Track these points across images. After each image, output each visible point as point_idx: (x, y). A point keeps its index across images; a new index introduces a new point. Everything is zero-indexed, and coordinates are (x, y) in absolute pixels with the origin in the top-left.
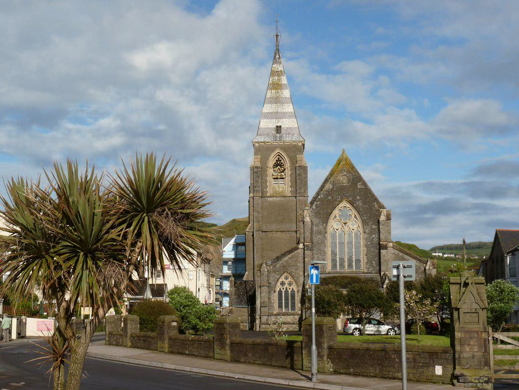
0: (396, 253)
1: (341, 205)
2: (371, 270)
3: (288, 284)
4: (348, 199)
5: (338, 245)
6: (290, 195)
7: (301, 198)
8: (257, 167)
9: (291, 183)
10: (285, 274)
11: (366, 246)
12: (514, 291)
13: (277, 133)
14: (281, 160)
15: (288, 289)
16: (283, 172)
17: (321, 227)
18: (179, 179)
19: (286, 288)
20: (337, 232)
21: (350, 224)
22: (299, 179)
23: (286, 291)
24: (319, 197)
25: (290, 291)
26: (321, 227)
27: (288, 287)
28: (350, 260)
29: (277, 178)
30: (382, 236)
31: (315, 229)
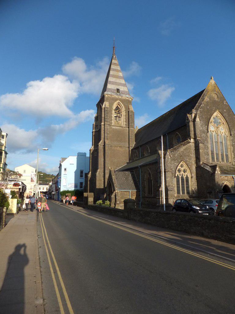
1: (215, 114)
3: (183, 171)
7: (132, 128)
9: (126, 120)
13: (117, 92)
15: (184, 176)
18: (104, 64)
19: (182, 174)
23: (182, 177)
24: (201, 106)
25: (185, 177)
27: (184, 174)
28: (222, 155)
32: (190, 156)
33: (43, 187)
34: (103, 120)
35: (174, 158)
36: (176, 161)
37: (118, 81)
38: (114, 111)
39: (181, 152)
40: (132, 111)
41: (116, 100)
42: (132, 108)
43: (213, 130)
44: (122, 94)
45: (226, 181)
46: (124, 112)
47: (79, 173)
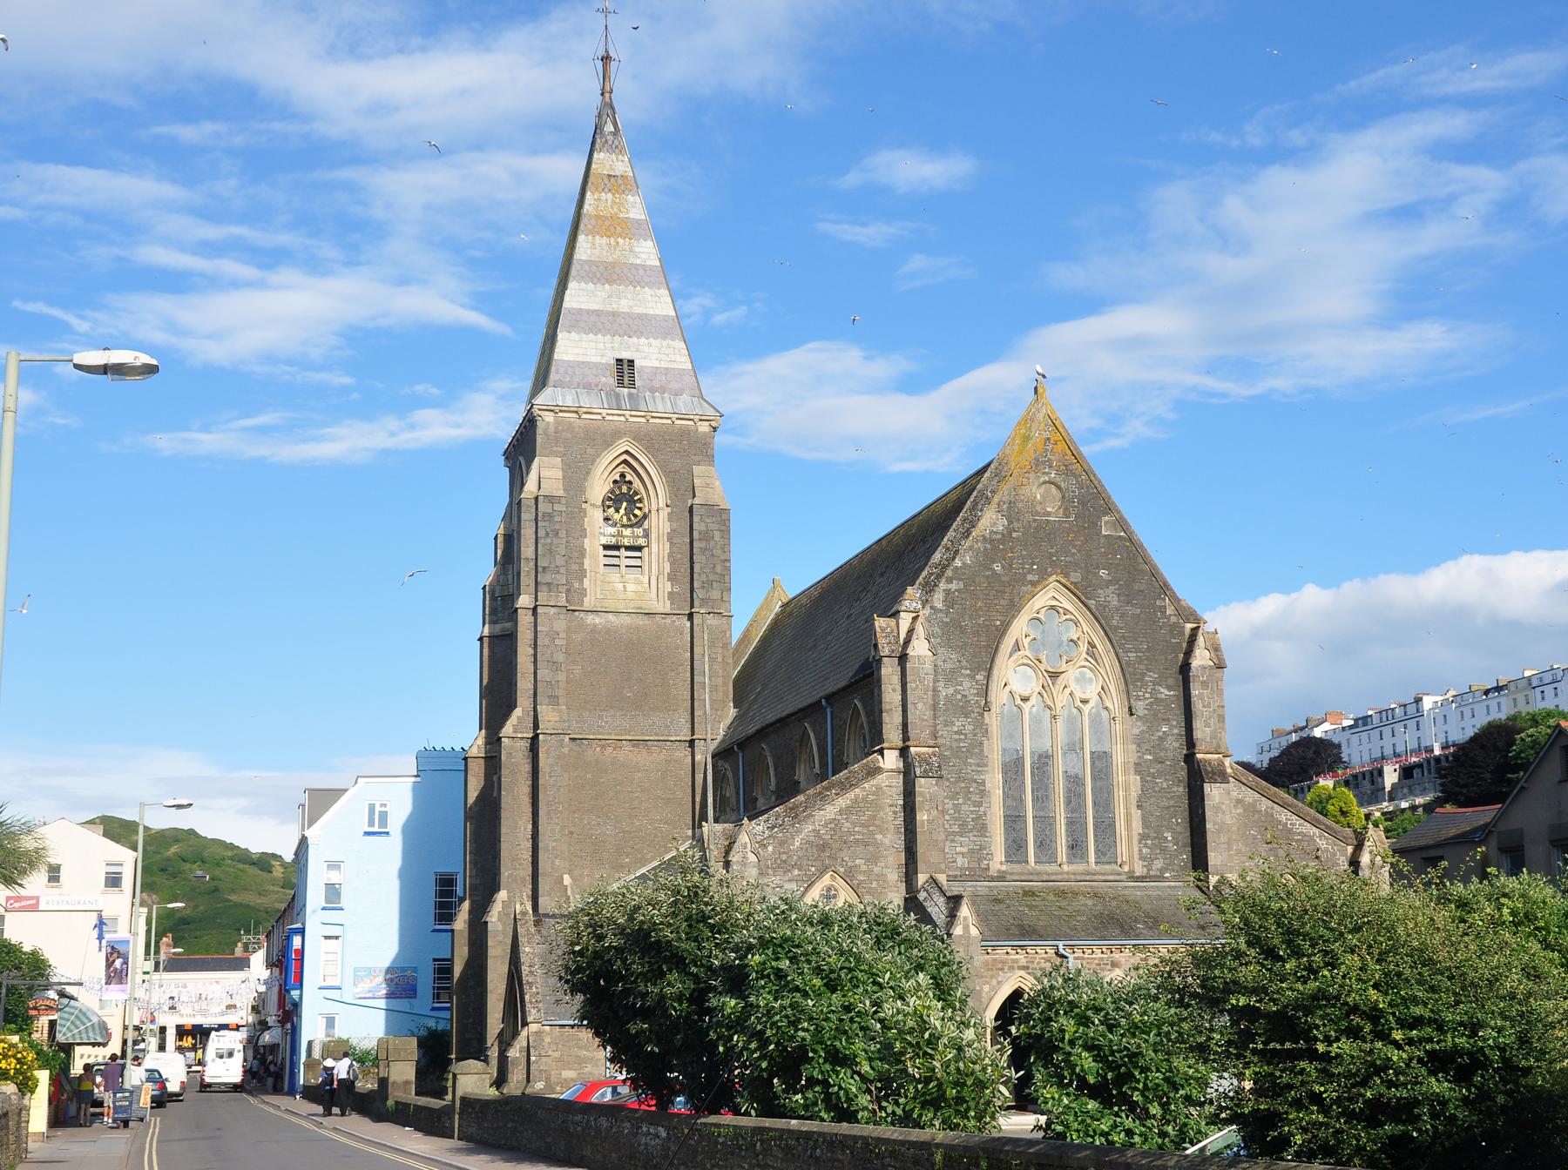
0: (1249, 800)
1: (1042, 600)
2: (1158, 864)
4: (1066, 575)
6: (668, 610)
7: (710, 620)
10: (826, 880)
11: (1139, 768)
12: (1192, 1049)
13: (631, 362)
14: (630, 483)
16: (639, 524)
17: (967, 687)
21: (1071, 675)
24: (958, 563)
26: (967, 684)
29: (616, 547)
30: (1201, 731)
32: (876, 844)
33: (1526, 693)
34: (527, 580)
35: (784, 857)
36: (796, 872)
37: (629, 301)
38: (598, 515)
39: (826, 825)
40: (708, 506)
41: (607, 438)
42: (712, 485)
43: (1026, 694)
44: (653, 390)
45: (1022, 973)
46: (665, 513)
47: (430, 896)
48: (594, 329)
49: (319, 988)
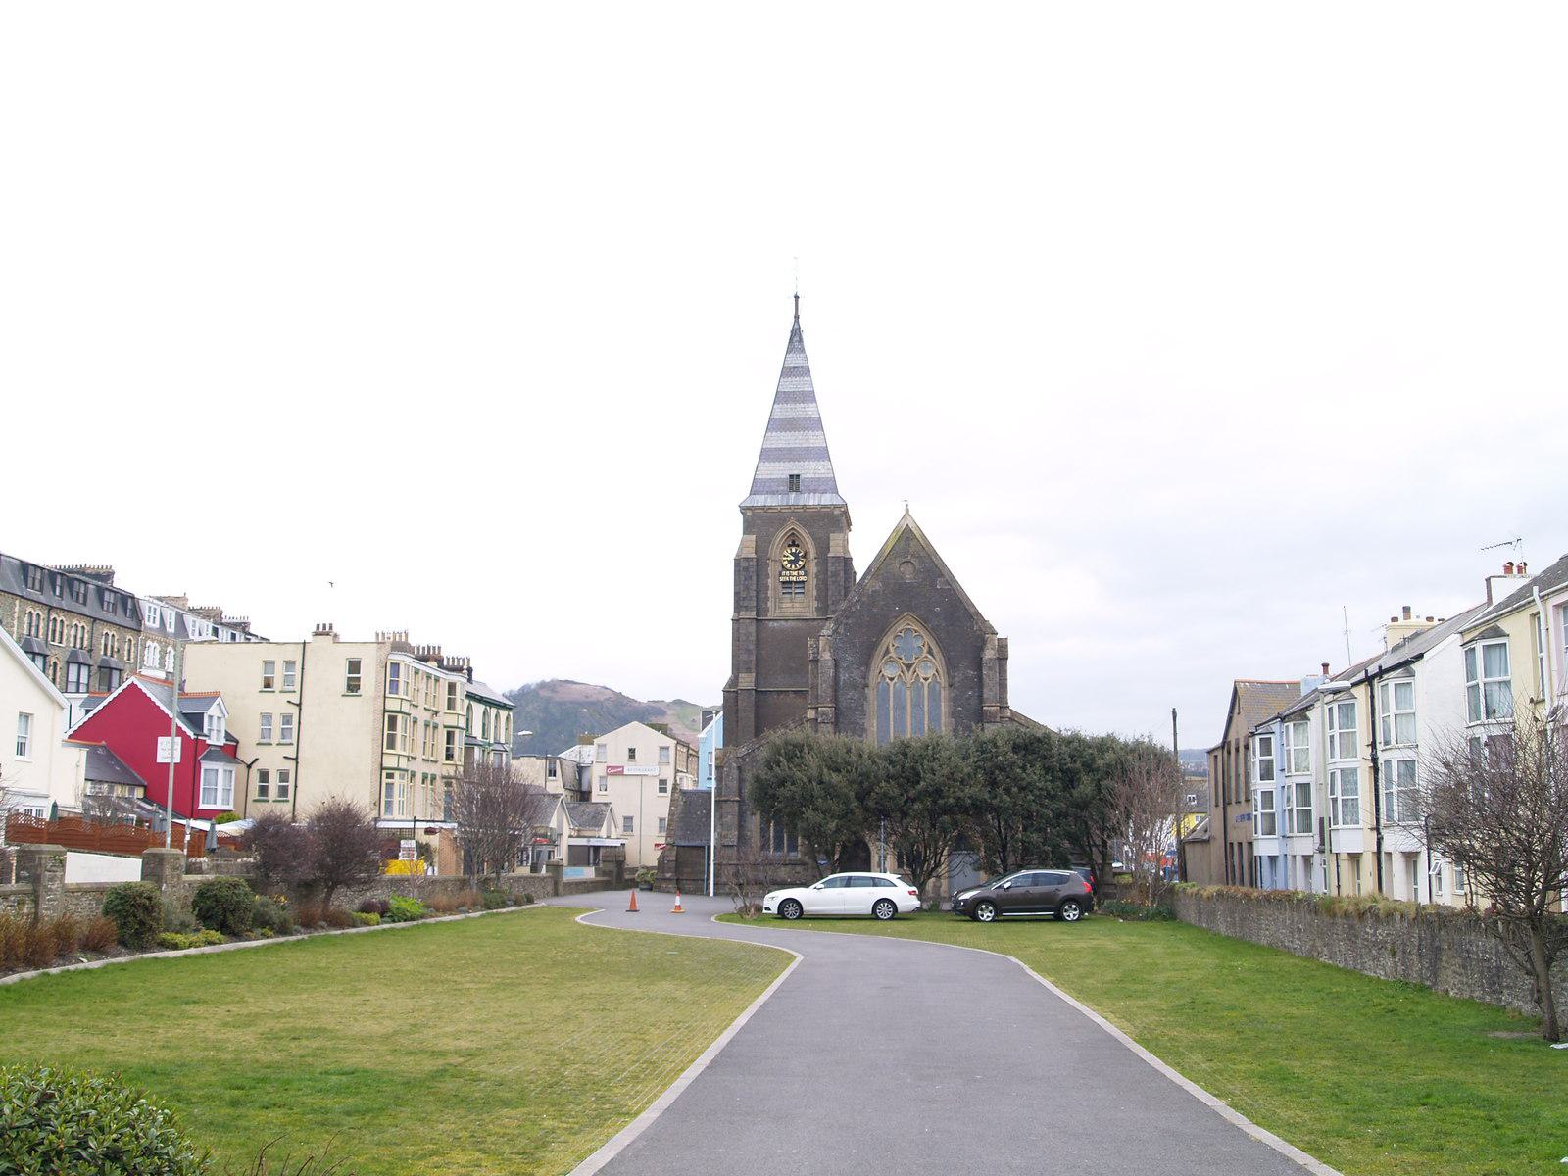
1: (901, 626)
5: (891, 712)
8: (747, 559)
11: (953, 714)
20: (891, 684)
22: (834, 582)
30: (986, 694)
31: (843, 677)
48: (779, 459)
49: (256, 759)
